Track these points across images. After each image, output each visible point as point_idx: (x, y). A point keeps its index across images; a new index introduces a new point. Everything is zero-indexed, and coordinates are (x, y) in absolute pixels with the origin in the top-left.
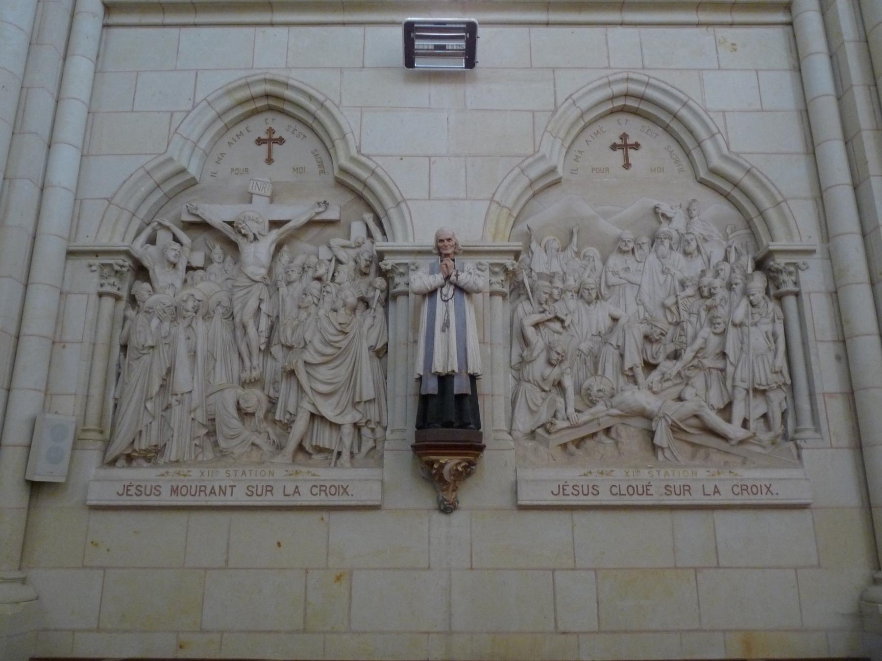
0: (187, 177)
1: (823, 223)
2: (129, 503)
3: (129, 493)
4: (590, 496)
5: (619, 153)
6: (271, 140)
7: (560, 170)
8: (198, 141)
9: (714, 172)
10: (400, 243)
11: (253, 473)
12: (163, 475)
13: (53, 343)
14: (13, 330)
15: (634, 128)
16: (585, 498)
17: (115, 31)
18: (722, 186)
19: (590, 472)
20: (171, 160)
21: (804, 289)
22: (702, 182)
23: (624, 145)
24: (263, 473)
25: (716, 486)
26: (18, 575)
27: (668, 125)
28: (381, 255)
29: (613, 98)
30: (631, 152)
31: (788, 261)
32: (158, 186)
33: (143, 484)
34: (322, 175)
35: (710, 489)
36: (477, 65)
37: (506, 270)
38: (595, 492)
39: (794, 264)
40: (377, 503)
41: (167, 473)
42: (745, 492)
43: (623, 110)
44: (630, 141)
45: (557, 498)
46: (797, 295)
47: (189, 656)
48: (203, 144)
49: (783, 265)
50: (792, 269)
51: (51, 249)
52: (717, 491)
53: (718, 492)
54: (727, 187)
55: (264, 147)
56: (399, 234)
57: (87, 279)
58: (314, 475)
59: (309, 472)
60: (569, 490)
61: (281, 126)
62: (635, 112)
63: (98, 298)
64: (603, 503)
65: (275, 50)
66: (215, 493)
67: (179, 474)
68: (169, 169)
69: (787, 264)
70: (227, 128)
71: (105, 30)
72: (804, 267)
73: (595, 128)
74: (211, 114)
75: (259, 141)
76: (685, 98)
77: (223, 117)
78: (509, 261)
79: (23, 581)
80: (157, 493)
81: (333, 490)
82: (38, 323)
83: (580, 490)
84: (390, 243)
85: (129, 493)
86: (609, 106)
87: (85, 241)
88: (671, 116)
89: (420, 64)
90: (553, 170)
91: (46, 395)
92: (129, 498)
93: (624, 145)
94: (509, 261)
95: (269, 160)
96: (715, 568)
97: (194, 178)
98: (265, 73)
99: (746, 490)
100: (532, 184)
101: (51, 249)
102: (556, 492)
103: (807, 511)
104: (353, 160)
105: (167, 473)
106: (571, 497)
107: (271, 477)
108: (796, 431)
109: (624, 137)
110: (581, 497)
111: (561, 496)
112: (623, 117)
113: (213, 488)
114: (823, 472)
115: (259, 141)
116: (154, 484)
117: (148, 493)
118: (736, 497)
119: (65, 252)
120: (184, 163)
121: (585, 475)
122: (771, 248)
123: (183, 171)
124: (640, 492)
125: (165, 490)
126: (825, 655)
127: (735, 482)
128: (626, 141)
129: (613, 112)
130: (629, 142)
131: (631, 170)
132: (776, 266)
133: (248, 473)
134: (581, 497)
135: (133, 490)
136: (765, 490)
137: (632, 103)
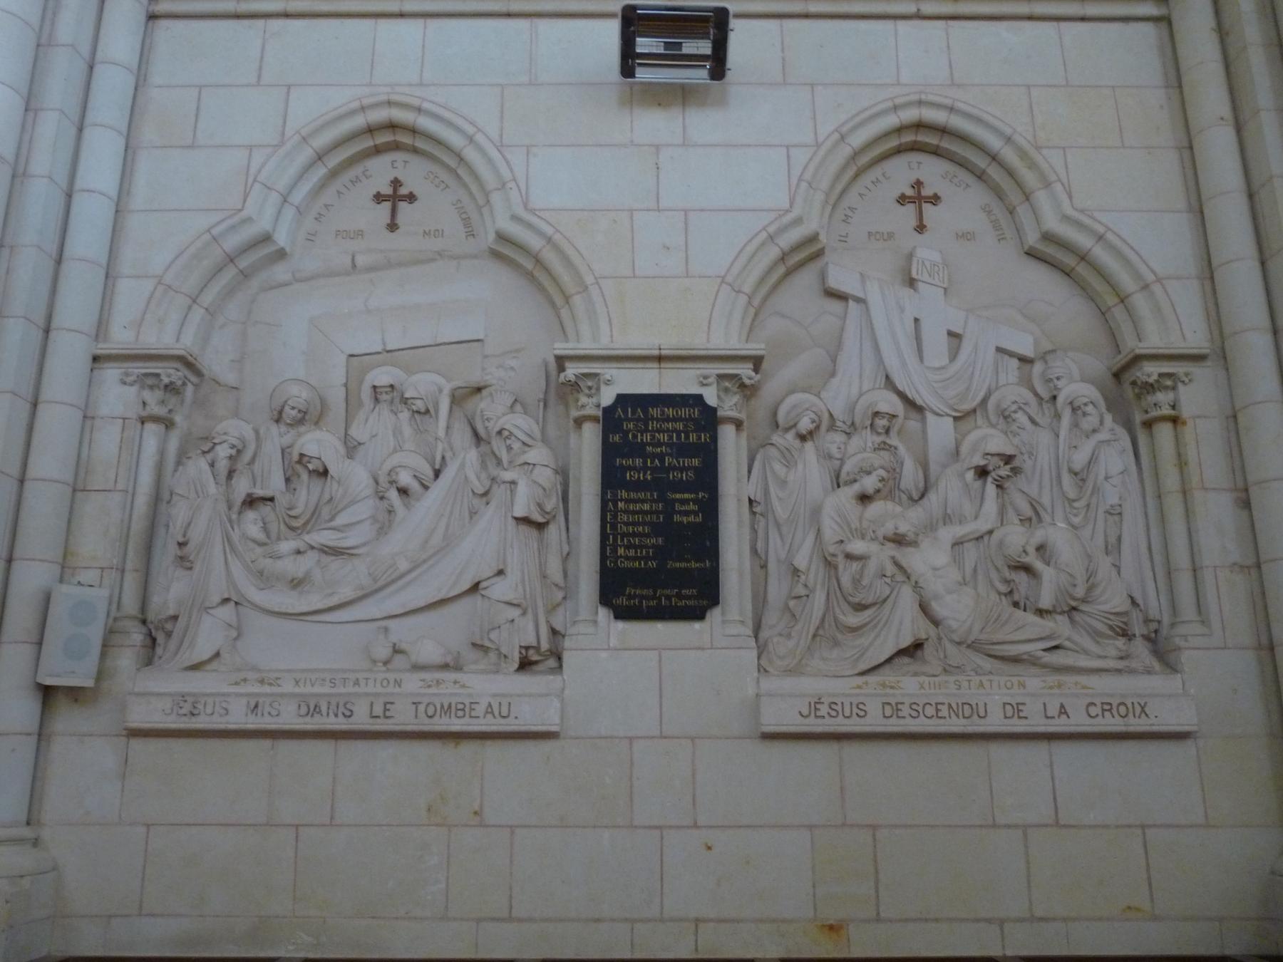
0: (819, 246)
1: (1213, 313)
2: (819, 729)
3: (900, 714)
4: (855, 719)
5: (910, 209)
6: (396, 197)
7: (822, 237)
8: (290, 192)
9: (1048, 237)
10: (586, 345)
11: (995, 684)
12: (859, 687)
13: (74, 490)
14: (15, 471)
15: (932, 172)
16: (846, 721)
17: (163, 23)
18: (1056, 256)
19: (245, 680)
20: (798, 221)
21: (1186, 411)
22: (1031, 254)
23: (918, 198)
24: (1009, 684)
25: (1062, 706)
26: (27, 832)
27: (984, 172)
28: (561, 361)
29: (900, 130)
30: (927, 207)
31: (722, 372)
32: (232, 261)
33: (838, 701)
34: (471, 239)
35: (1053, 710)
36: (729, 75)
37: (743, 386)
38: (862, 713)
39: (1170, 375)
40: (554, 729)
41: (866, 683)
42: (1107, 714)
43: (915, 148)
44: (927, 192)
45: (807, 721)
46: (1175, 420)
47: (326, 956)
48: (298, 197)
49: (1155, 377)
50: (1169, 383)
51: (69, 354)
52: (1063, 711)
53: (1066, 713)
54: (1069, 260)
55: (387, 206)
56: (585, 329)
57: (117, 396)
58: (463, 686)
59: (1076, 684)
60: (906, 711)
61: (414, 173)
62: (936, 152)
63: (139, 425)
64: (287, 727)
65: (399, 61)
66: (492, 713)
67: (884, 685)
68: (795, 235)
69: (1160, 375)
70: (334, 174)
71: (150, 23)
72: (1187, 380)
73: (876, 172)
74: (307, 154)
75: (379, 198)
76: (470, 130)
77: (325, 159)
78: (745, 371)
79: (36, 842)
80: (914, 707)
81: (1123, 710)
82: (50, 462)
83: (839, 708)
84: (570, 345)
85: (900, 714)
86: (893, 143)
87: (121, 337)
88: (989, 159)
89: (643, 75)
90: (813, 238)
91: (63, 567)
92: (820, 721)
93: (918, 198)
94: (745, 371)
95: (393, 227)
96: (816, 826)
97: (283, 249)
98: (921, 92)
99: (1110, 710)
100: (783, 258)
101: (69, 354)
102: (805, 712)
103: (1190, 742)
104: (515, 218)
105: (866, 683)
106: (828, 720)
107: (397, 690)
108: (1173, 625)
109: (918, 184)
110: (840, 719)
111: (812, 720)
112: (915, 157)
113: (490, 705)
114: (1209, 682)
115: (379, 198)
116: (855, 701)
117: (847, 713)
118: (1092, 721)
119: (90, 359)
120: (264, 224)
121: (859, 687)
122: (1138, 351)
123: (266, 238)
124: (847, 713)
125: (874, 708)
126: (1214, 951)
127: (1089, 700)
128: (919, 192)
129: (899, 151)
130: (925, 192)
131: (926, 235)
132: (1145, 378)
133: (362, 683)
134: (840, 719)
135: (824, 710)
136: (1138, 710)
137: (932, 139)
